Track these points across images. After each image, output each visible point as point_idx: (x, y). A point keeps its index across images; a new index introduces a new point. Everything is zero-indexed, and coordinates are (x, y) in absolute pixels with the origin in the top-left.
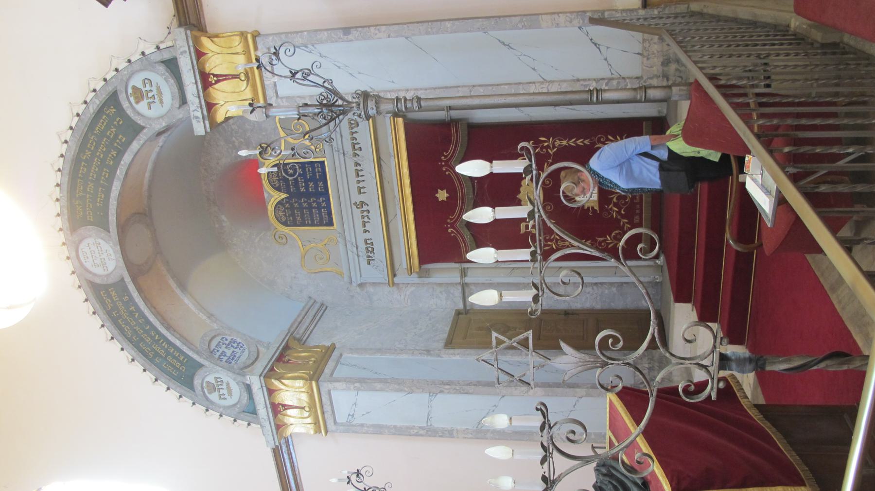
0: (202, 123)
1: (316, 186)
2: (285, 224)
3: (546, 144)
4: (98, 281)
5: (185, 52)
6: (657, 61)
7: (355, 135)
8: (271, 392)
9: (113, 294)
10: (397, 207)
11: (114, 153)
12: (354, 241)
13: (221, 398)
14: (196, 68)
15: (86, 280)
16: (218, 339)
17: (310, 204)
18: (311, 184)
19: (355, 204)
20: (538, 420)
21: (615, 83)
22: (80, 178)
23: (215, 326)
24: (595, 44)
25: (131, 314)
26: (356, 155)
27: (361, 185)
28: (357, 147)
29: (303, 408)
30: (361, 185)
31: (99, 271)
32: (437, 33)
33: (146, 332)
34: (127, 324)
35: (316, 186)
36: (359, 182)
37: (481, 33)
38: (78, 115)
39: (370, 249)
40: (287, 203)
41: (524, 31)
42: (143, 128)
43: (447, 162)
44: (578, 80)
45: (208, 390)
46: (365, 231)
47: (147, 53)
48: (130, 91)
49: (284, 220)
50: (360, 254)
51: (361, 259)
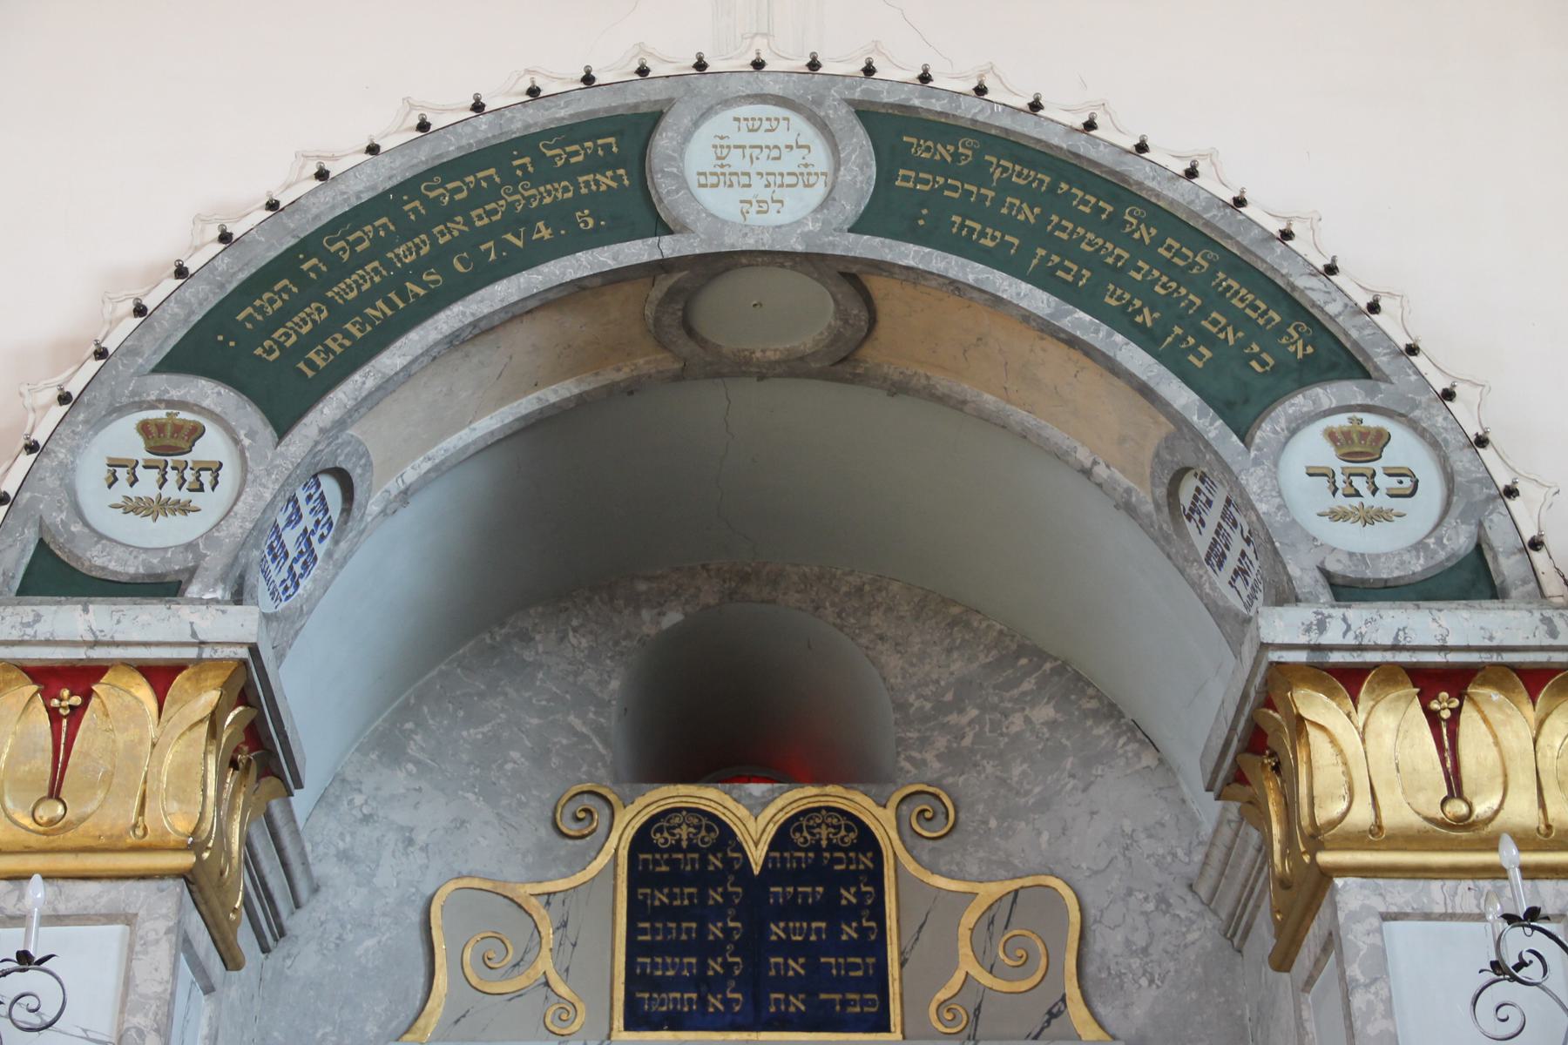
0: (1303, 640)
2: (641, 841)
4: (663, 142)
5: (1553, 633)
8: (160, 676)
9: (606, 181)
11: (1147, 318)
13: (114, 464)
14: (1495, 658)
15: (670, 102)
17: (716, 949)
18: (796, 967)
22: (1053, 188)
23: (373, 508)
25: (522, 221)
29: (55, 793)
31: (699, 156)
33: (440, 257)
34: (479, 197)
35: (788, 985)
38: (1286, 235)
40: (728, 862)
42: (1244, 435)
45: (160, 426)
47: (1513, 504)
48: (1371, 421)
49: (658, 838)
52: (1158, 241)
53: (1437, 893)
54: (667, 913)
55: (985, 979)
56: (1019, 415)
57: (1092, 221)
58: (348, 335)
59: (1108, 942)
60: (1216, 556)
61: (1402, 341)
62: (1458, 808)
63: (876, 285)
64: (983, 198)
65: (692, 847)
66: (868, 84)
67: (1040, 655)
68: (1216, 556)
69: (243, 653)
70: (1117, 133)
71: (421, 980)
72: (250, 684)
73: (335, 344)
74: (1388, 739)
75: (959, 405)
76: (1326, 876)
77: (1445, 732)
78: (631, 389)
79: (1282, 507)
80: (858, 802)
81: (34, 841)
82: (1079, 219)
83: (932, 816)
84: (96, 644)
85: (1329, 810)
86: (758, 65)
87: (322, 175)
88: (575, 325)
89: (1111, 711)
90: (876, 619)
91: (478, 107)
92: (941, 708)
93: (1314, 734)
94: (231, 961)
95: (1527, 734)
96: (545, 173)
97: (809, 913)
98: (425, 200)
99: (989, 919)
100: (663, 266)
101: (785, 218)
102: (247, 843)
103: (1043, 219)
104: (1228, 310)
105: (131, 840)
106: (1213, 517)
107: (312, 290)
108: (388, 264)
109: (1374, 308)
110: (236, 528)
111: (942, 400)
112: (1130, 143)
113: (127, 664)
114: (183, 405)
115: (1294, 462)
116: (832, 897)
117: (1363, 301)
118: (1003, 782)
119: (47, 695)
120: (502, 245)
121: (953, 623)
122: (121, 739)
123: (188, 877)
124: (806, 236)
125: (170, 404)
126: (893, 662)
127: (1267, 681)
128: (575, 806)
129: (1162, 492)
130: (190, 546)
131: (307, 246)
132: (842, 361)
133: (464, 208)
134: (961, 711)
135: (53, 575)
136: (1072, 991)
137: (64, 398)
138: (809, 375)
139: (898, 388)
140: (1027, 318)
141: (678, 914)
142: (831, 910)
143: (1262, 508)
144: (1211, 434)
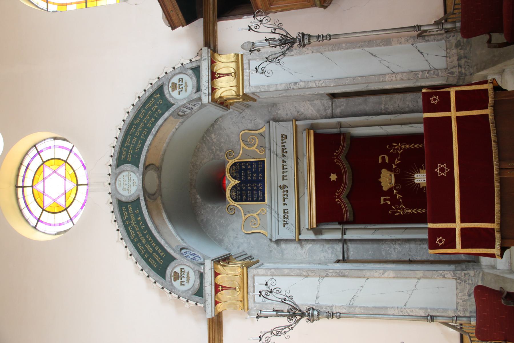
3: (396, 147)
4: (123, 199)
5: (206, 59)
6: (455, 58)
7: (284, 144)
8: (216, 274)
9: (130, 209)
10: (306, 187)
11: (153, 120)
12: (277, 210)
13: (181, 285)
15: (116, 198)
16: (186, 250)
17: (252, 188)
18: (255, 175)
19: (280, 186)
21: (432, 72)
22: (130, 135)
23: (185, 244)
24: (421, 53)
25: (138, 222)
26: (283, 156)
28: (285, 151)
29: (235, 289)
30: (285, 174)
31: (126, 193)
32: (338, 49)
33: (144, 235)
34: (133, 229)
36: (283, 172)
37: (360, 50)
38: (139, 97)
39: (286, 216)
40: (238, 186)
41: (383, 47)
42: (173, 105)
43: (337, 156)
44: (412, 72)
45: (174, 278)
46: (285, 204)
48: (170, 85)
49: (235, 198)
50: (279, 219)
51: (280, 223)
52: (140, 118)
55: (256, 145)
56: (167, 140)
57: (136, 129)
58: (158, 249)
59: (250, 126)
60: (191, 109)
61: (157, 80)
62: (233, 74)
63: (147, 164)
64: (132, 147)
65: (236, 192)
66: (113, 166)
67: (203, 136)
68: (191, 109)
69: (213, 262)
70: (121, 125)
71: (258, 234)
72: (217, 261)
73: (160, 251)
74: (222, 84)
75: (165, 150)
76: (244, 94)
77: (221, 75)
78: (163, 204)
79: (185, 99)
80: (228, 166)
81: (242, 291)
82: (136, 131)
83: (230, 154)
84: (211, 284)
85: (234, 93)
86: (109, 184)
87: (131, 255)
89: (213, 125)
90: (198, 163)
91: (118, 230)
93: (222, 95)
94: (258, 262)
95: (221, 63)
96: (129, 219)
97: (246, 173)
98: (134, 238)
99: (247, 145)
100: (145, 199)
102: (241, 260)
103: (136, 137)
104: (152, 107)
105: (242, 276)
106: (185, 109)
107: (151, 256)
108: (146, 243)
109: (151, 84)
110: (191, 265)
111: (165, 153)
112: (123, 123)
113: (214, 280)
114: (171, 275)
116: (244, 170)
117: (150, 86)
118: (225, 143)
119: (219, 291)
120: (142, 225)
122: (226, 279)
123: (247, 268)
124: (140, 175)
125: (171, 277)
127: (214, 102)
128: (230, 211)
129: (181, 117)
130: (194, 272)
131: (143, 257)
132: (158, 169)
133: (136, 232)
134: (213, 149)
135: (200, 292)
137: (170, 293)
138: (161, 174)
139: (163, 160)
140: (153, 139)
141: (247, 194)
142: (246, 170)
143: (185, 102)
144: (173, 110)
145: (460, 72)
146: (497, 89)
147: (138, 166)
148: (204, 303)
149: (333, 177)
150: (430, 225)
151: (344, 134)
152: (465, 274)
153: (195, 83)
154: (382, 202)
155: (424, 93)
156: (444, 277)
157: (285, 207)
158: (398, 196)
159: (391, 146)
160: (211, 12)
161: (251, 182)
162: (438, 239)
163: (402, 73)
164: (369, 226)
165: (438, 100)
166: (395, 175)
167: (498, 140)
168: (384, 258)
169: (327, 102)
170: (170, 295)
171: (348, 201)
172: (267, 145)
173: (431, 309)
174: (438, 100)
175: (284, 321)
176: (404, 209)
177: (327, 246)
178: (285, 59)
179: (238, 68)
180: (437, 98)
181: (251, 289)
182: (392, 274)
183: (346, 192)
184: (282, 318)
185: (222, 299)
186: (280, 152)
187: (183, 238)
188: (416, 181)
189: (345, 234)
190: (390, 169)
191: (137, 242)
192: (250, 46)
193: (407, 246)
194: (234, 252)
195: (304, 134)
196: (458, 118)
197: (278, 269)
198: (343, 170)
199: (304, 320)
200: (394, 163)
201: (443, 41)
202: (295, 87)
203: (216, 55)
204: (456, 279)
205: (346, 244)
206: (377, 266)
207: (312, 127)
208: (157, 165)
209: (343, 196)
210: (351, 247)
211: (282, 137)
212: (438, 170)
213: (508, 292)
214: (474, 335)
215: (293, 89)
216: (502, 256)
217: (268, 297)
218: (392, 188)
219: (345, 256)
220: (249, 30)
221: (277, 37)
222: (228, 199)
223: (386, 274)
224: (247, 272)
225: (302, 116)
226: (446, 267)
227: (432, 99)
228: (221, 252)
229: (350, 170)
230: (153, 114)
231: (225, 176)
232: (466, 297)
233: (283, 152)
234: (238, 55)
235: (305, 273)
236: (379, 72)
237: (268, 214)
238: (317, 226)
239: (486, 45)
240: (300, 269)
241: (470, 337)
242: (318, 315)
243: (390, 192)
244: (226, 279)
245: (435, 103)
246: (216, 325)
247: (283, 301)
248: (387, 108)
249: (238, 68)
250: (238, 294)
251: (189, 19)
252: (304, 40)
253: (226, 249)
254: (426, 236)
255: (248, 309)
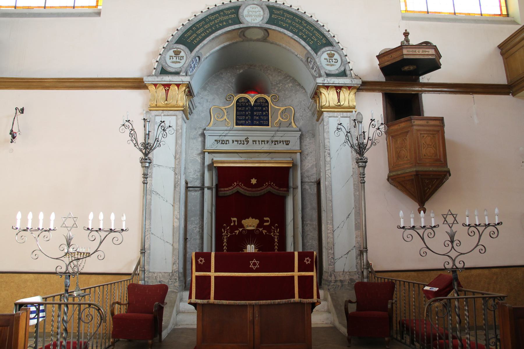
1: (256, 120)
2: (237, 101)
4: (241, 10)
6: (342, 278)
8: (178, 85)
9: (233, 16)
11: (305, 37)
13: (170, 56)
15: (242, 5)
17: (247, 115)
18: (257, 118)
19: (248, 138)
20: (477, 224)
21: (333, 261)
25: (221, 22)
26: (272, 142)
27: (257, 142)
29: (166, 100)
30: (257, 142)
31: (245, 12)
32: (354, 188)
33: (211, 27)
34: (216, 18)
35: (256, 120)
36: (259, 141)
37: (353, 206)
38: (323, 26)
39: (223, 142)
41: (354, 224)
42: (316, 54)
43: (270, 185)
45: (176, 51)
46: (233, 141)
48: (333, 52)
52: (307, 26)
53: (336, 114)
54: (241, 111)
55: (282, 120)
56: (288, 47)
57: (298, 23)
59: (297, 115)
60: (313, 68)
62: (339, 104)
63: (269, 31)
67: (290, 77)
68: (313, 68)
70: (302, 11)
73: (198, 39)
75: (280, 46)
76: (323, 112)
77: (338, 94)
78: (236, 43)
80: (266, 97)
82: (296, 22)
83: (276, 99)
85: (324, 104)
87: (195, 16)
88: (229, 35)
89: (299, 85)
90: (269, 71)
91: (216, 6)
92: (277, 84)
96: (225, 15)
97: (259, 111)
99: (282, 112)
100: (241, 28)
101: (257, 22)
102: (189, 105)
103: (291, 22)
106: (312, 63)
107: (194, 32)
109: (334, 37)
110: (186, 65)
111: (278, 45)
112: (303, 12)
115: (322, 58)
119: (165, 88)
120: (219, 25)
121: (279, 72)
122: (174, 93)
126: (271, 77)
130: (180, 68)
131: (194, 26)
132: (264, 40)
133: (214, 20)
135: (164, 72)
136: (293, 121)
137: (164, 48)
139: (272, 43)
140: (289, 36)
142: (262, 111)
145: (331, 281)
146: (313, 305)
147: (267, 23)
148: (155, 75)
149: (254, 181)
150: (213, 254)
151: (288, 191)
152: (176, 279)
153: (333, 73)
154: (233, 219)
155: (313, 253)
156: (174, 264)
157: (231, 142)
158: (237, 232)
159: (277, 228)
160: (390, 88)
161: (251, 115)
162: (203, 259)
163: (333, 238)
164: (214, 208)
165: (307, 263)
166: (253, 230)
167: (275, 304)
168: (188, 219)
169: (314, 179)
170: (162, 47)
171: (234, 192)
172: (281, 129)
173: (150, 253)
174: (307, 263)
175: (141, 140)
176: (227, 236)
177: (199, 174)
178: (348, 147)
179: (344, 108)
180: (309, 262)
181: (166, 113)
182: (176, 224)
183: (242, 191)
184: (144, 138)
185: (158, 89)
186: (276, 139)
187: (208, 59)
188: (248, 246)
189: (208, 189)
190: (259, 226)
191: (205, 21)
192: (359, 120)
193: (198, 237)
194: (196, 99)
195: (289, 159)
196: (293, 277)
197: (182, 135)
198: (259, 189)
199: (142, 156)
200: (263, 229)
201: (356, 270)
202: (326, 153)
203: (355, 90)
204: (172, 273)
205: (200, 190)
206: (183, 213)
207: (295, 165)
208: (268, 38)
209: (238, 189)
210: (198, 194)
211: (288, 141)
212: (255, 261)
213: (163, 308)
214: (131, 282)
215: (325, 152)
216: (190, 303)
217: (160, 127)
218: (244, 227)
219: (191, 189)
220: (371, 120)
221: (365, 141)
222: (241, 95)
223: (176, 220)
224: (180, 110)
225: (304, 158)
226: (181, 266)
227: (308, 258)
228: (195, 89)
229: (258, 195)
230: (309, 37)
231: (259, 93)
232: (158, 279)
233: (275, 141)
234: (354, 108)
235: (178, 156)
236: (335, 219)
237: (226, 128)
238: (215, 167)
239: (348, 300)
240: (181, 152)
241: (130, 280)
242: (146, 167)
243: (241, 225)
244: (174, 93)
245: (305, 261)
246: (137, 84)
247: (157, 140)
248: (307, 225)
249: (344, 108)
250: (162, 103)
251: (384, 69)
252: (361, 162)
253: (198, 93)
254: (205, 251)
255: (150, 110)
